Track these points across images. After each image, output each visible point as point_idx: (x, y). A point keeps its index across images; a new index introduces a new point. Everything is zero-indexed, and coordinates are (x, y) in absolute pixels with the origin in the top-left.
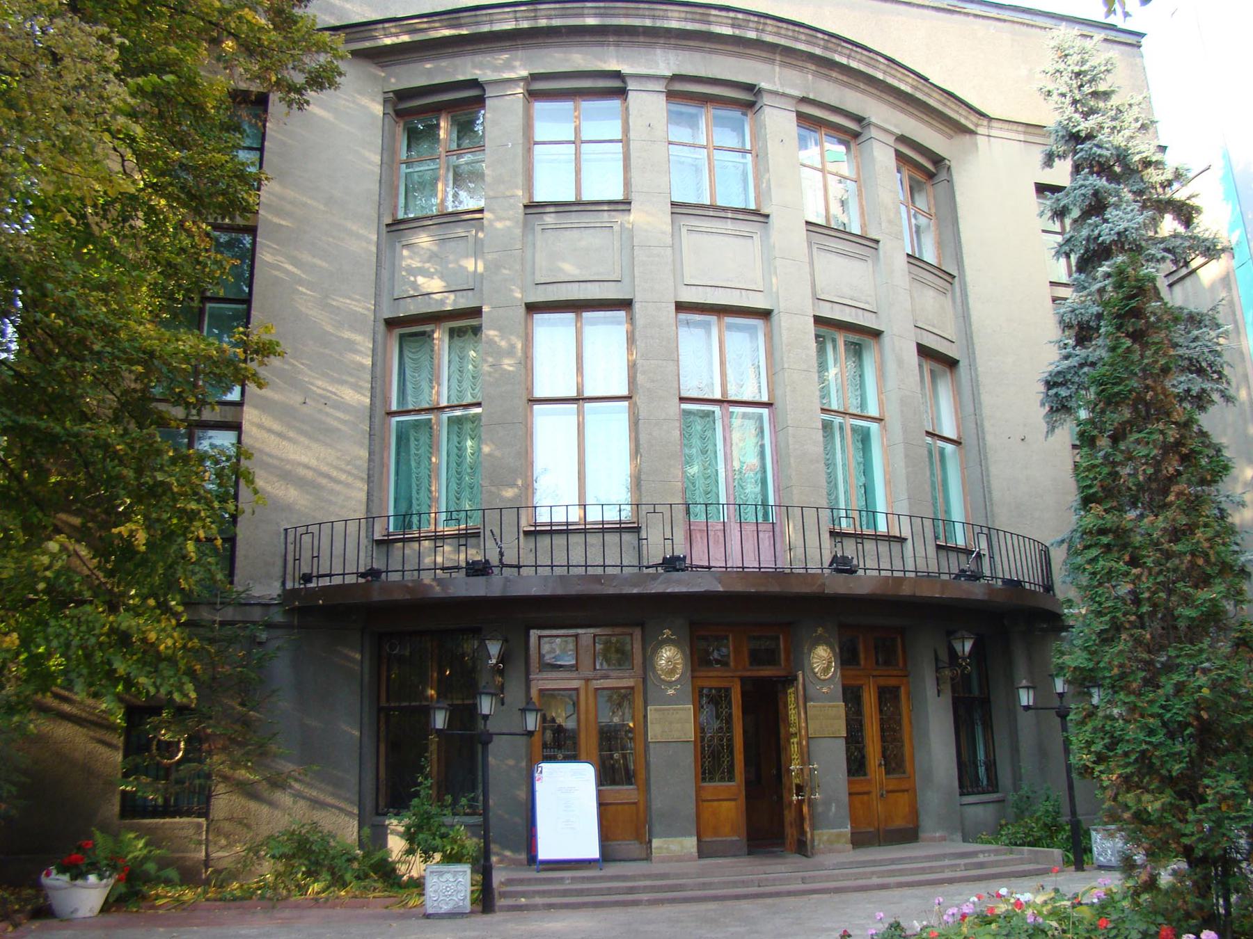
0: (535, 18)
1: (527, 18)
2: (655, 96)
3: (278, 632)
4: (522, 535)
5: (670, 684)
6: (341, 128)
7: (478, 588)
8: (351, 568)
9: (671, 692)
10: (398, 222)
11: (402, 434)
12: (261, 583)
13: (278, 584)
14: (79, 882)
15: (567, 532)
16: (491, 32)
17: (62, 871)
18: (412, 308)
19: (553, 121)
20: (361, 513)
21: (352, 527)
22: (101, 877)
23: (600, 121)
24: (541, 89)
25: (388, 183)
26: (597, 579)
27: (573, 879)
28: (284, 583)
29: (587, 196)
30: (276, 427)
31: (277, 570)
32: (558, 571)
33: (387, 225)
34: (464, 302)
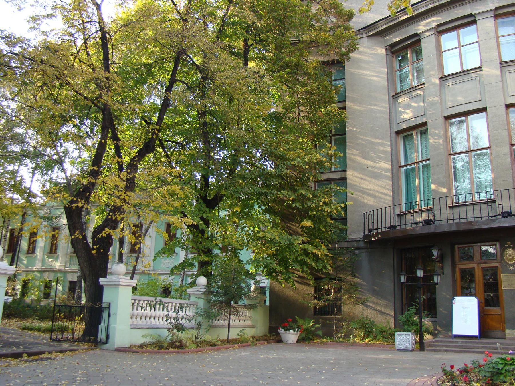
0: (427, 6)
1: (431, 4)
2: (488, 19)
3: (363, 251)
4: (448, 208)
5: (511, 265)
6: (369, 63)
7: (431, 229)
8: (384, 226)
9: (512, 268)
10: (396, 94)
11: (405, 174)
12: (355, 233)
13: (362, 234)
14: (288, 332)
15: (466, 205)
16: (418, 13)
17: (283, 328)
18: (404, 126)
19: (449, 40)
20: (391, 204)
21: (388, 209)
22: (294, 331)
23: (469, 35)
24: (441, 30)
25: (391, 80)
26: (470, 223)
27: (462, 342)
28: (364, 233)
29: (465, 69)
30: (360, 176)
31: (362, 229)
32: (456, 221)
33: (392, 96)
34: (420, 121)
